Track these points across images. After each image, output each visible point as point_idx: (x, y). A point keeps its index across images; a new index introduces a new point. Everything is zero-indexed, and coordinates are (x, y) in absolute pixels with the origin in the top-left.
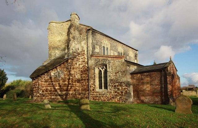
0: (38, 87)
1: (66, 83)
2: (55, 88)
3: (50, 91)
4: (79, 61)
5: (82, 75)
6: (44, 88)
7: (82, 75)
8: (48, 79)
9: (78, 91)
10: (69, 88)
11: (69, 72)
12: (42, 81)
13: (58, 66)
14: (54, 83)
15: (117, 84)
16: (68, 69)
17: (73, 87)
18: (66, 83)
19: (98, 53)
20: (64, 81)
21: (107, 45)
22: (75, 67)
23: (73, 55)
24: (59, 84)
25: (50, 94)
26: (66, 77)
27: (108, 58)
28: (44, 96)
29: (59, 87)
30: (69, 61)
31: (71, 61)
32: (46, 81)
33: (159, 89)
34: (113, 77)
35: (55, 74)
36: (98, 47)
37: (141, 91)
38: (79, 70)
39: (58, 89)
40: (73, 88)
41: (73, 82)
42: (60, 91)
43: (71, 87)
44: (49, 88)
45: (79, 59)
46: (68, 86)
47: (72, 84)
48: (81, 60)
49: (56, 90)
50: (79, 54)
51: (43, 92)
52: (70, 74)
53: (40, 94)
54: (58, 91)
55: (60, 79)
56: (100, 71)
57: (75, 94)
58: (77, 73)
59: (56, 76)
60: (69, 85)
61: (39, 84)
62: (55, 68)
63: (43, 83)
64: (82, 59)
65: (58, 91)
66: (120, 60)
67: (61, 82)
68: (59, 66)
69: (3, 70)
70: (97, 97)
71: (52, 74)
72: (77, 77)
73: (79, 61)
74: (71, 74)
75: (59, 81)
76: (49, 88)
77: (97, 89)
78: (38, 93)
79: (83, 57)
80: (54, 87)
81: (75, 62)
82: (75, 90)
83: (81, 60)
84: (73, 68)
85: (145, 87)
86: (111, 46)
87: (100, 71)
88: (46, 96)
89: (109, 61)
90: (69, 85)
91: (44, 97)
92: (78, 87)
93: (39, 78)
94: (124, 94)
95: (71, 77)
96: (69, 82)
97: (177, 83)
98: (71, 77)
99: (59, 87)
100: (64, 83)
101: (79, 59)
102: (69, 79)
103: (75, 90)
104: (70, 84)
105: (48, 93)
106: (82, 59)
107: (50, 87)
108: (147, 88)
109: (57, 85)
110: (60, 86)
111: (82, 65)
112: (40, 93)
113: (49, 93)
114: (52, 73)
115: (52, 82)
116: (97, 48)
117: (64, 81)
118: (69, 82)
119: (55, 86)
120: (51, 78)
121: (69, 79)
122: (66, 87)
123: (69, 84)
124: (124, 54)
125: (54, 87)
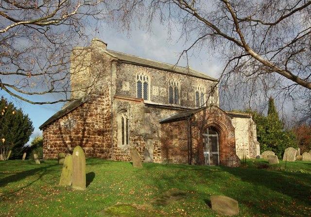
0: (46, 141)
1: (80, 135)
2: (65, 143)
3: (60, 146)
4: (103, 105)
5: (106, 123)
6: (53, 142)
7: (106, 123)
8: (57, 131)
9: (99, 147)
10: (84, 142)
11: (85, 120)
12: (50, 133)
13: (69, 113)
14: (64, 136)
15: (136, 137)
16: (83, 116)
17: (91, 141)
18: (80, 135)
19: (128, 92)
20: (77, 133)
21: (146, 79)
22: (93, 113)
23: (91, 97)
24: (70, 137)
25: (59, 149)
26: (80, 127)
27: (128, 101)
28: (52, 153)
29: (70, 141)
30: (85, 105)
31: (88, 106)
32: (55, 133)
33: (187, 144)
34: (133, 128)
35: (65, 123)
36: (128, 84)
37: (170, 148)
38: (101, 117)
39: (69, 144)
40: (90, 142)
41: (89, 134)
42: (72, 146)
43: (87, 141)
44: (58, 142)
45: (103, 102)
46: (82, 140)
47: (89, 137)
48: (105, 103)
49: (66, 146)
50: (103, 95)
51: (51, 147)
52: (85, 124)
53: (48, 150)
54: (69, 146)
55: (72, 130)
56: (123, 119)
57: (94, 152)
58: (97, 121)
59: (67, 126)
60: (85, 139)
61: (47, 137)
62: (65, 115)
63: (52, 135)
64: (106, 101)
65: (69, 146)
66: (139, 104)
67: (73, 135)
68: (70, 113)
69: (27, 116)
70: (120, 155)
71: (62, 123)
72: (98, 127)
73: (103, 105)
74: (87, 123)
75: (70, 133)
76: (58, 142)
77: (120, 146)
78: (47, 148)
79: (107, 99)
80: (63, 140)
81: (94, 106)
82: (93, 146)
83: (105, 103)
84: (91, 115)
85: (174, 142)
86: (152, 80)
87: (123, 119)
88: (55, 153)
89: (129, 105)
90: (85, 139)
91: (52, 155)
92: (99, 141)
93: (48, 129)
94: (142, 151)
95: (87, 128)
96: (83, 134)
97: (229, 137)
98: (87, 128)
99: (70, 141)
100: (76, 136)
101: (103, 102)
102: (84, 130)
103: (93, 146)
104: (86, 137)
105: (57, 149)
106: (106, 101)
107: (59, 140)
108: (175, 143)
109: (68, 138)
110: (71, 140)
111: (107, 110)
112: (49, 148)
113: (58, 148)
114: (62, 123)
115: (61, 133)
116: (126, 86)
117: (77, 133)
118: (83, 134)
119: (65, 139)
120: (60, 129)
121: (84, 130)
122: (79, 142)
123: (84, 137)
124: (182, 89)
125: (63, 140)
